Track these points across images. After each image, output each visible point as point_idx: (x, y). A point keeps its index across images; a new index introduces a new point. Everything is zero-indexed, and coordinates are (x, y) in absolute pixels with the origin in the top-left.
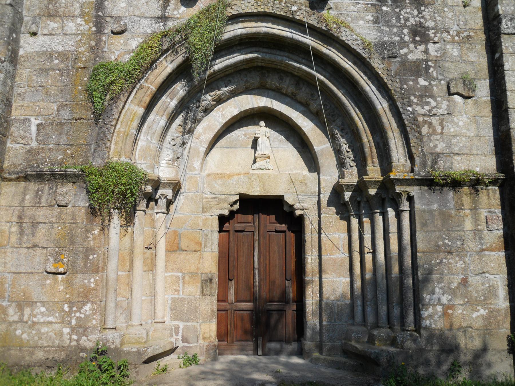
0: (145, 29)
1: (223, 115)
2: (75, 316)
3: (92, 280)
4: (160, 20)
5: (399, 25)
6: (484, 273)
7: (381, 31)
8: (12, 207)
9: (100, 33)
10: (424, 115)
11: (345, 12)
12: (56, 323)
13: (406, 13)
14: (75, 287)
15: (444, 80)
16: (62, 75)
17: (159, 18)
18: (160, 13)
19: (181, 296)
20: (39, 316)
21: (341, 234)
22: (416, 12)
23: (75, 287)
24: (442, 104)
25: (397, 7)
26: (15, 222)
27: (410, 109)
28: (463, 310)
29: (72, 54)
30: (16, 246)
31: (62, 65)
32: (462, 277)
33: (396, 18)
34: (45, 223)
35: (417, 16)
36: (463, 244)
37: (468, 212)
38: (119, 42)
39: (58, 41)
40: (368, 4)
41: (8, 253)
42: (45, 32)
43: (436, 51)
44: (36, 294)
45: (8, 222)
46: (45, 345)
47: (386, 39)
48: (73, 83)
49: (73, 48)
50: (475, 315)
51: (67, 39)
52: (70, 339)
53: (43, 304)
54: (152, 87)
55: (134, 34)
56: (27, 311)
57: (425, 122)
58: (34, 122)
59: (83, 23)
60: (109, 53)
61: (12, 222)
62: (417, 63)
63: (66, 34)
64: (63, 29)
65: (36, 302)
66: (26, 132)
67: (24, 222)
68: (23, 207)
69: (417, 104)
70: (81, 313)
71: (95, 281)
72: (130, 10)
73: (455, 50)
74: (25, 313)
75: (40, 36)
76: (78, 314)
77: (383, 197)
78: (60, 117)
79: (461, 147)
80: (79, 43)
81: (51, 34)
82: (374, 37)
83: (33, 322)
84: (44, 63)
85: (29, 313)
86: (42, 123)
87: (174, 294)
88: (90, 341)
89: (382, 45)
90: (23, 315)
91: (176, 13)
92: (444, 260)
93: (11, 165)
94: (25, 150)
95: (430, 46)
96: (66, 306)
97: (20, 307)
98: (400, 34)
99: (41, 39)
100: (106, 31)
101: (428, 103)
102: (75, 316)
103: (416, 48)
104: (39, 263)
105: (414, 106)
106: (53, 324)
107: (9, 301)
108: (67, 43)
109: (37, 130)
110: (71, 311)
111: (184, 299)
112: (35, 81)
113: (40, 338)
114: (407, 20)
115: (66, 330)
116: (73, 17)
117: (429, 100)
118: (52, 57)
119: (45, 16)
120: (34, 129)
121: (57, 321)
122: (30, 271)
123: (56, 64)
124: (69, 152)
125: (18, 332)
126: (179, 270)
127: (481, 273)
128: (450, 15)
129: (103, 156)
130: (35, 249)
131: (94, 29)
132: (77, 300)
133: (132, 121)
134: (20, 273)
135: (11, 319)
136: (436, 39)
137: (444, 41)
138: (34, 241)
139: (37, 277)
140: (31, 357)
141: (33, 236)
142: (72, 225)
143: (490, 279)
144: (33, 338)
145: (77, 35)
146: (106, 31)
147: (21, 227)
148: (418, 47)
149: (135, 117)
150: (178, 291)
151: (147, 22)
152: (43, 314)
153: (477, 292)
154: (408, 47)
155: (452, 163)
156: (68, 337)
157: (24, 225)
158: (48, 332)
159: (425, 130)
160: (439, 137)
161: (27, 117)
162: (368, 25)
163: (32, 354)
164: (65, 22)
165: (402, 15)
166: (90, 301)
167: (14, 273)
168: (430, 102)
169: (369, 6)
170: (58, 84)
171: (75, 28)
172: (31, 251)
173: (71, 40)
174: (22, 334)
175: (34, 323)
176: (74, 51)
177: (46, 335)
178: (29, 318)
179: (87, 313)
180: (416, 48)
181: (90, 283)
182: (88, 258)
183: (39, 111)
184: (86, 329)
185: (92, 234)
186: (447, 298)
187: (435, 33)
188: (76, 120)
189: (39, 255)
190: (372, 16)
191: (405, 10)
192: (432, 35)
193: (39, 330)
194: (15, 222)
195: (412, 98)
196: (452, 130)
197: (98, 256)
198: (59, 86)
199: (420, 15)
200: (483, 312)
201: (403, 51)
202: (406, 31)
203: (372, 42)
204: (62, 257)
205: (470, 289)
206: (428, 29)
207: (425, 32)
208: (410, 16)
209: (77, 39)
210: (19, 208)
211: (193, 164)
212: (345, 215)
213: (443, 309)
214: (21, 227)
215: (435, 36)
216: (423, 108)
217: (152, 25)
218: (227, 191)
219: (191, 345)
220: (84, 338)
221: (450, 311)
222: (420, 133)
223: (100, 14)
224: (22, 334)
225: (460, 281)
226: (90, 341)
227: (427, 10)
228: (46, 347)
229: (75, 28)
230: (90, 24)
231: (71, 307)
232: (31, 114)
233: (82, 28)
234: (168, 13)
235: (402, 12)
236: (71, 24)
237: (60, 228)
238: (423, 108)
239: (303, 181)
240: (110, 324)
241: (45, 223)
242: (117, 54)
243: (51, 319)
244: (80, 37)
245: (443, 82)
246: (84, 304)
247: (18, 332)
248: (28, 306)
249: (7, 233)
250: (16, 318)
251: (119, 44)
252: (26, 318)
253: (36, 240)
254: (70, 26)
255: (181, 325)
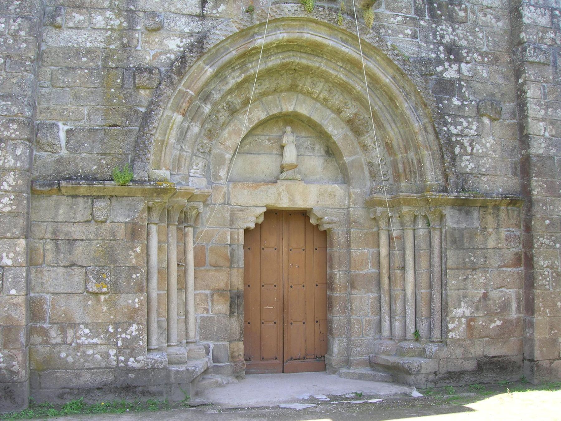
0: (182, 28)
1: (249, 119)
2: (121, 337)
3: (137, 300)
4: (198, 19)
5: (435, 41)
6: (501, 287)
7: (419, 47)
8: (45, 222)
9: (133, 29)
10: (457, 135)
11: (385, 24)
12: (101, 344)
13: (442, 29)
14: (119, 307)
15: (475, 101)
16: (91, 75)
17: (196, 16)
18: (198, 11)
19: (211, 314)
20: (83, 339)
21: (370, 250)
22: (450, 30)
23: (119, 307)
24: (473, 125)
25: (434, 22)
26: (49, 239)
27: (445, 129)
28: (483, 322)
29: (101, 52)
30: (52, 265)
31: (91, 64)
32: (483, 291)
33: (433, 34)
34: (82, 240)
35: (452, 34)
36: (485, 261)
37: (490, 230)
38: (154, 41)
39: (85, 36)
40: (407, 17)
41: (45, 273)
42: (71, 24)
43: (468, 71)
44: (78, 315)
45: (42, 239)
46: (93, 367)
47: (424, 55)
48: (105, 85)
49: (103, 44)
50: (492, 326)
51: (95, 34)
52: (118, 361)
53: (86, 325)
54: (191, 92)
55: (170, 33)
56: (70, 333)
57: (458, 142)
58: (63, 128)
59: (114, 17)
60: (143, 52)
61: (46, 239)
62: (451, 81)
63: (94, 29)
64: (90, 23)
65: (79, 324)
66: (54, 138)
67: (59, 239)
68: (57, 222)
69: (451, 124)
70: (127, 334)
71: (140, 301)
72: (165, 5)
73: (484, 71)
74: (68, 335)
75: (65, 29)
76: (123, 335)
77: (416, 214)
78: (92, 122)
79: (487, 168)
80: (109, 41)
81: (77, 28)
82: (412, 52)
83: (77, 343)
84: (71, 61)
85: (72, 335)
86: (72, 129)
87: (203, 313)
88: (138, 362)
89: (420, 61)
90: (65, 337)
91: (214, 12)
92: (470, 276)
93: (40, 176)
94: (53, 159)
95: (463, 65)
96: (111, 327)
97: (63, 330)
98: (437, 52)
99: (65, 33)
100: (138, 28)
101: (461, 124)
102: (121, 337)
103: (450, 66)
104: (79, 282)
105: (449, 125)
106: (99, 347)
107: (50, 323)
108: (96, 38)
109: (67, 137)
110: (116, 332)
111: (214, 317)
112: (61, 81)
113: (86, 361)
114: (442, 37)
115: (113, 352)
116: (101, 9)
117: (462, 120)
118: (79, 54)
119: (70, 7)
120: (62, 135)
121: (102, 343)
122: (69, 291)
123: (84, 63)
124: (104, 162)
125: (63, 355)
126: (206, 287)
127: (499, 288)
128: (480, 35)
129: (144, 167)
130: (73, 268)
131: (125, 24)
132: (123, 321)
133: (171, 129)
134: (60, 293)
135: (54, 341)
136: (468, 59)
137: (476, 61)
138: (72, 259)
139: (78, 298)
140: (79, 379)
141: (70, 254)
142: (112, 242)
143: (506, 293)
144: (79, 360)
145: (107, 30)
146: (138, 28)
147: (57, 244)
148: (453, 66)
149: (174, 125)
150: (207, 310)
151: (183, 20)
152: (86, 335)
153: (495, 305)
154: (444, 65)
155: (478, 183)
156: (115, 358)
157: (59, 242)
158: (94, 354)
159: (457, 150)
160: (468, 158)
161: (54, 121)
162: (407, 39)
163: (78, 376)
164: (93, 15)
165: (438, 31)
166: (135, 321)
167: (53, 293)
168: (462, 122)
169: (408, 19)
170: (88, 85)
171: (104, 22)
172: (69, 270)
173: (100, 36)
174: (67, 356)
175: (79, 346)
176: (104, 48)
177: (91, 357)
178: (73, 340)
179: (133, 334)
180: (450, 66)
181: (134, 303)
182: (131, 277)
183: (68, 115)
184: (133, 349)
185: (134, 252)
186: (471, 311)
187: (468, 53)
188: (110, 126)
189: (78, 275)
190: (411, 30)
191: (440, 27)
192: (465, 55)
193: (84, 353)
194: (49, 239)
195: (447, 117)
196: (480, 151)
197: (141, 275)
198: (88, 88)
199: (455, 33)
200: (498, 323)
201: (440, 69)
202: (441, 48)
203: (412, 57)
204: (104, 276)
205: (490, 302)
206: (461, 48)
207: (458, 51)
208: (445, 33)
209: (107, 35)
210: (52, 223)
211: (219, 172)
212: (374, 230)
213: (467, 321)
214: (57, 244)
215: (468, 56)
216: (456, 128)
217: (189, 23)
218: (254, 203)
219: (222, 364)
220: (132, 359)
221: (472, 323)
222: (453, 153)
223: (132, 7)
224: (67, 356)
225: (481, 295)
226: (138, 362)
227: (460, 28)
228: (93, 369)
229: (104, 22)
230: (120, 19)
231: (116, 328)
232: (58, 118)
233: (112, 22)
234: (207, 11)
235: (438, 29)
236: (100, 18)
237: (98, 245)
238: (456, 128)
239: (332, 194)
240: (154, 344)
241: (82, 240)
242: (152, 54)
243: (95, 340)
244: (109, 32)
245: (473, 103)
246: (130, 325)
247: (63, 355)
248: (71, 328)
249: (42, 250)
250: (59, 340)
251: (154, 43)
252: (69, 340)
253: (74, 259)
254: (99, 20)
255: (212, 344)
